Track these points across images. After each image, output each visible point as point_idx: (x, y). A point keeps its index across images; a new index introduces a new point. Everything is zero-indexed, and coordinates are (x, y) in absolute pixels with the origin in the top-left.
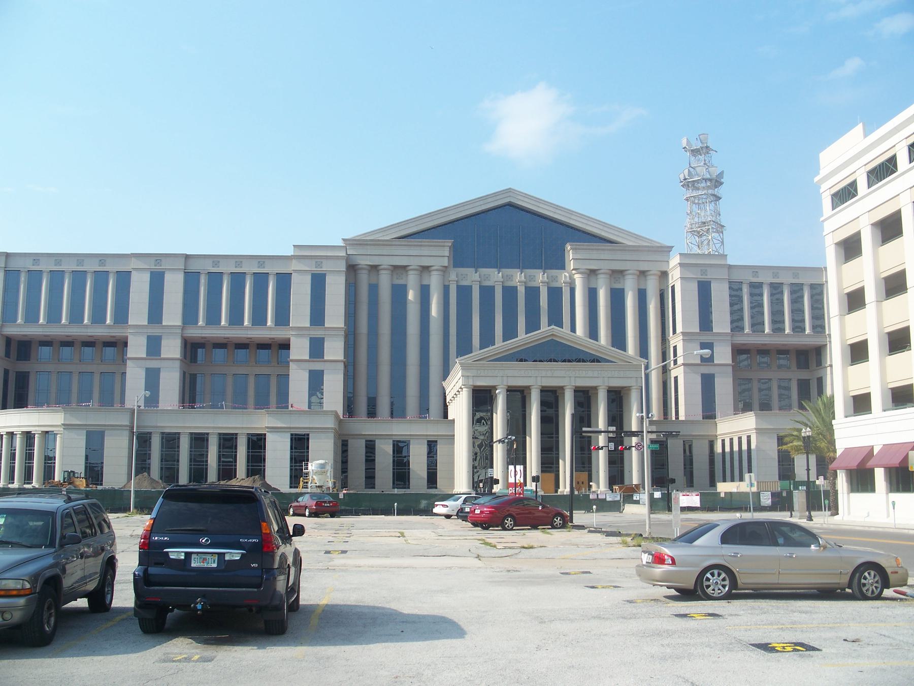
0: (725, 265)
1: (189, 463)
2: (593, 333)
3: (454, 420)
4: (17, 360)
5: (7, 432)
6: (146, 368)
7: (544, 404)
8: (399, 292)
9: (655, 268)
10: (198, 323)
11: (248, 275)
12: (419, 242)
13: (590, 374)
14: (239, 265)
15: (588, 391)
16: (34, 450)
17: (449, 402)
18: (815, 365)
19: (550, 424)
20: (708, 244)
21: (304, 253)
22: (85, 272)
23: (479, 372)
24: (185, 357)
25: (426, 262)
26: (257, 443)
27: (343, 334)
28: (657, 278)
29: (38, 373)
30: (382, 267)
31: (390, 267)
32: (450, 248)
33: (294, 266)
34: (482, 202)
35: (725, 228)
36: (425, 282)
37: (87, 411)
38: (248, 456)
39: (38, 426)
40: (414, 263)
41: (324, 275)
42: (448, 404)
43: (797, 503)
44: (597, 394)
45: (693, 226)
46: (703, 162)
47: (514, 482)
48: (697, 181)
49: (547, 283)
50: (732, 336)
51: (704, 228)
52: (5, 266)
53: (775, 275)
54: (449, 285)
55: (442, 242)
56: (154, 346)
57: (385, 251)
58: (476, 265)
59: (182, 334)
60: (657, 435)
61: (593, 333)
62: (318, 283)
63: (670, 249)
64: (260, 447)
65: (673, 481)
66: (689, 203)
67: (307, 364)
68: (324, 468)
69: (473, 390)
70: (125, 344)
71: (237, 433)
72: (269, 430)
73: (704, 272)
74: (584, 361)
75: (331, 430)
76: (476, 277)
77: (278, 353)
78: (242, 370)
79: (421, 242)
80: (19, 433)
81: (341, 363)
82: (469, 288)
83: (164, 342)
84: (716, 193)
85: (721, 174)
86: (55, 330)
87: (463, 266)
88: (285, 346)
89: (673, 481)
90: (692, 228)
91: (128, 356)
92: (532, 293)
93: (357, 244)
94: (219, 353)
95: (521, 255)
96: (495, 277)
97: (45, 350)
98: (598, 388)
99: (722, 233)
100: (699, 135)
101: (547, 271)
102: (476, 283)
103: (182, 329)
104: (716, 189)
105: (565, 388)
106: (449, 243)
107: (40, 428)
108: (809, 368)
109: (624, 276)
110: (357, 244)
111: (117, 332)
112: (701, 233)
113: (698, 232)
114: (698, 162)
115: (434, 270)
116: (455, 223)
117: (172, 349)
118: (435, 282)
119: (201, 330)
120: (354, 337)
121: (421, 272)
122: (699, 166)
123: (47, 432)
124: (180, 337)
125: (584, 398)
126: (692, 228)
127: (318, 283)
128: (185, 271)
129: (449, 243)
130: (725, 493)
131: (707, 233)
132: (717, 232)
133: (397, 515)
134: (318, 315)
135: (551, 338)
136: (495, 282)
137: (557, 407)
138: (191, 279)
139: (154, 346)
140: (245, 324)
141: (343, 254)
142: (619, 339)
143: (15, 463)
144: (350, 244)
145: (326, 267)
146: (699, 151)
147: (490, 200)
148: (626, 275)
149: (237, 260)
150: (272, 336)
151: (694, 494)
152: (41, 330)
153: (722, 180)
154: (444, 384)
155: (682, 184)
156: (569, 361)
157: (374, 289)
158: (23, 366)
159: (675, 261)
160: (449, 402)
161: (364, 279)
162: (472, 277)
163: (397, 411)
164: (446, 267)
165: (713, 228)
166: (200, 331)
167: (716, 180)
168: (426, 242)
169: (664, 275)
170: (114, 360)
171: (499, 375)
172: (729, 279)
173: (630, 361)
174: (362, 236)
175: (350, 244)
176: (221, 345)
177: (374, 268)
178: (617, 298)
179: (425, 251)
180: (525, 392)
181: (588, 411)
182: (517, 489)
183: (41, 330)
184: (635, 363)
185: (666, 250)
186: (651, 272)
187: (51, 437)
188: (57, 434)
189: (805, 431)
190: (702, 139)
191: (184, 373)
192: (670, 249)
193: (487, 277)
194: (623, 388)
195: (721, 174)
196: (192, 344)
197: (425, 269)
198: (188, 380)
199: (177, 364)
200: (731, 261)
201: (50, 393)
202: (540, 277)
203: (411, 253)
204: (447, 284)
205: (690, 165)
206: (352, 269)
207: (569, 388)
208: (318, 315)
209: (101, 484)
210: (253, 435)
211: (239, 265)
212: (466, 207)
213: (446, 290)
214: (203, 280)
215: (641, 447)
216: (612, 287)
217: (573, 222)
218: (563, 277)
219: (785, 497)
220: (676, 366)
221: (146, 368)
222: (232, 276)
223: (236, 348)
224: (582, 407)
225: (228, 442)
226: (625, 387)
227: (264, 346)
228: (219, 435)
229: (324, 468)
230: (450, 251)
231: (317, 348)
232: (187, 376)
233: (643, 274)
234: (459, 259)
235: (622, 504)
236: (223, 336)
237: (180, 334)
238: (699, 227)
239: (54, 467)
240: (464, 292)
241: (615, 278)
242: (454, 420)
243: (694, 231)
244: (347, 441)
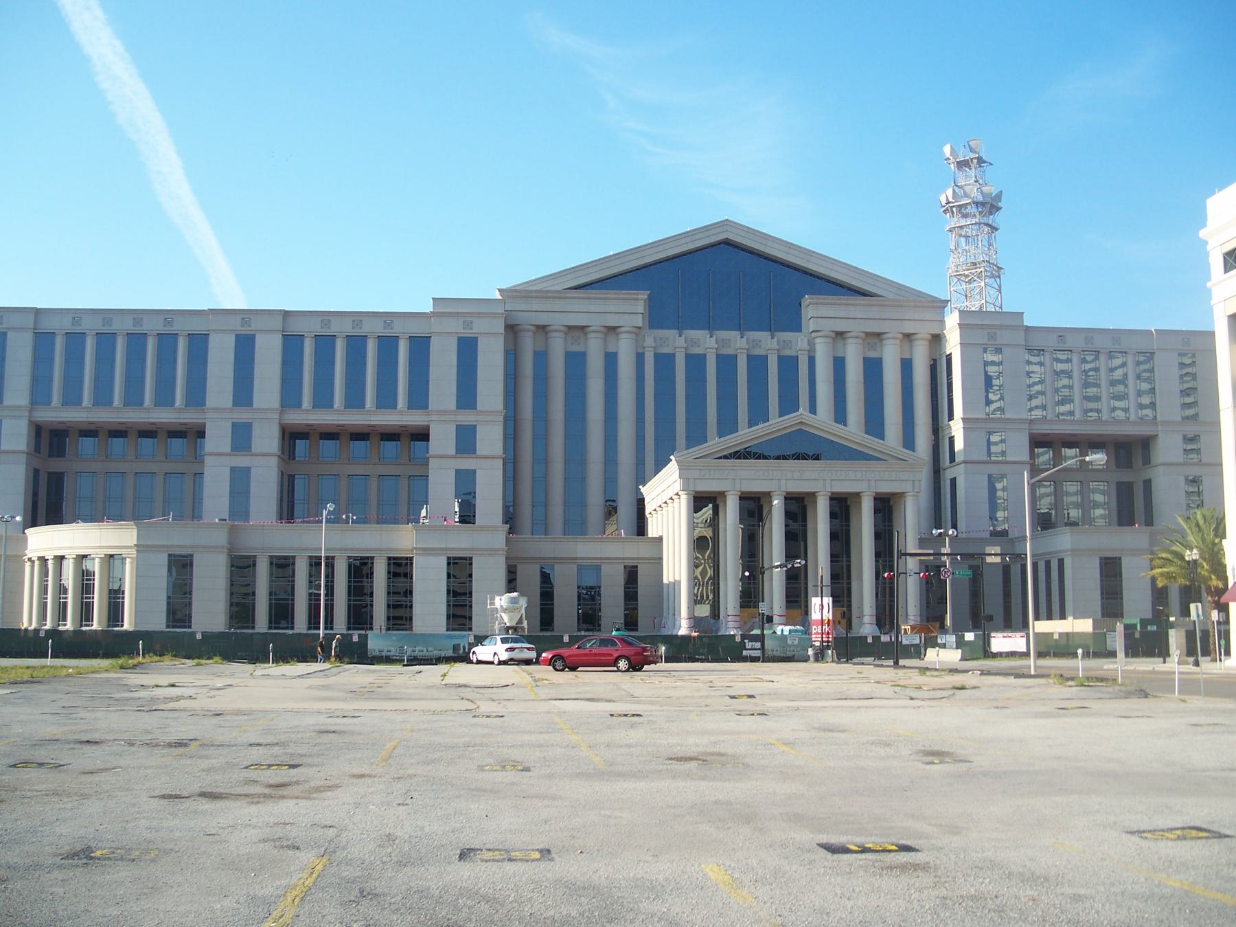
0: (1020, 326)
1: (308, 598)
2: (840, 415)
3: (660, 539)
4: (50, 456)
5: (54, 556)
6: (456, 470)
7: (789, 515)
8: (576, 363)
9: (924, 331)
10: (113, 403)
11: (308, 339)
12: (604, 293)
13: (851, 475)
14: (468, 325)
15: (846, 499)
16: (94, 580)
17: (650, 513)
18: (1140, 462)
19: (796, 540)
20: (980, 293)
21: (446, 308)
22: (364, 338)
23: (766, 474)
24: (37, 449)
25: (612, 321)
26: (400, 568)
27: (502, 420)
28: (926, 343)
29: (79, 474)
30: (591, 329)
31: (602, 329)
32: (645, 302)
33: (436, 326)
34: (688, 239)
35: (1002, 271)
36: (611, 349)
37: (342, 530)
38: (349, 587)
39: (100, 547)
40: (595, 322)
41: (253, 337)
42: (648, 516)
43: (1175, 644)
44: (860, 503)
45: (960, 268)
46: (974, 179)
47: (820, 618)
48: (965, 206)
49: (778, 350)
50: (1029, 423)
51: (973, 271)
52: (283, 328)
53: (388, 325)
54: (644, 353)
55: (634, 294)
56: (242, 437)
57: (558, 305)
58: (680, 325)
59: (280, 420)
60: (1002, 558)
61: (840, 415)
62: (467, 349)
63: (944, 305)
64: (1115, 576)
65: (990, 618)
66: (954, 235)
67: (452, 461)
68: (517, 603)
69: (694, 497)
70: (201, 434)
71: (374, 557)
72: (418, 552)
73: (468, 325)
74: (765, 458)
75: (222, 550)
76: (681, 341)
77: (196, 444)
78: (359, 470)
79: (606, 294)
80: (99, 556)
81: (274, 457)
82: (672, 357)
83: (256, 431)
84: (990, 222)
85: (999, 196)
86: (132, 415)
87: (662, 328)
88: (422, 435)
89: (990, 618)
90: (957, 271)
91: (206, 450)
92: (758, 364)
93: (517, 297)
94: (329, 446)
95: (711, 309)
96: (707, 342)
97: (88, 444)
98: (817, 494)
99: (1000, 278)
100: (968, 142)
101: (745, 333)
102: (773, 352)
103: (280, 414)
104: (991, 217)
105: (771, 494)
106: (644, 295)
107: (102, 550)
108: (1132, 467)
109: (881, 340)
110: (517, 297)
111: (190, 417)
112: (970, 278)
113: (967, 276)
114: (967, 179)
115: (889, 338)
116: (651, 267)
117: (267, 439)
118: (625, 349)
119: (307, 415)
120: (514, 424)
121: (606, 334)
122: (969, 185)
123: (112, 556)
124: (278, 424)
125: (842, 507)
126: (957, 271)
127: (467, 349)
128: (284, 333)
129: (644, 295)
130: (1060, 634)
131: (979, 277)
132: (993, 276)
133: (665, 662)
134: (467, 395)
135: (798, 428)
136: (768, 350)
137: (805, 519)
138: (292, 344)
139: (242, 437)
140: (367, 407)
141: (501, 310)
142: (874, 424)
143: (47, 598)
144: (509, 297)
145: (479, 327)
146: (969, 163)
147: (699, 236)
148: (884, 339)
149: (467, 319)
150: (404, 423)
151: (1018, 635)
152: (84, 415)
153: (1000, 204)
154: (643, 489)
155: (944, 209)
156: (785, 458)
157: (541, 358)
158: (56, 465)
159: (952, 321)
160: (650, 513)
161: (528, 345)
162: (676, 342)
163: (576, 526)
164: (639, 328)
165: (986, 271)
166: (54, 414)
167: (992, 204)
168: (612, 294)
169: (937, 339)
170: (124, 455)
171: (729, 477)
172: (1026, 346)
173: (904, 458)
174: (522, 286)
175: (509, 297)
176: (330, 434)
177: (542, 329)
178: (873, 369)
179: (612, 306)
180: (806, 500)
181: (846, 526)
182: (824, 627)
183: (84, 415)
184: (911, 461)
185: (940, 305)
186: (919, 336)
187: (117, 562)
188: (125, 558)
189: (1190, 553)
190: (973, 146)
191: (282, 473)
192: (944, 305)
193: (756, 343)
194: (893, 494)
195: (999, 196)
196: (51, 431)
197: (612, 330)
198: (286, 483)
199: (23, 458)
200: (1028, 321)
201: (154, 502)
202: (767, 343)
203: (592, 308)
204: (640, 351)
205: (955, 183)
206: (512, 330)
207: (867, 495)
208: (467, 395)
209: (292, 628)
210: (355, 558)
211: (326, 324)
212: (667, 246)
213: (640, 358)
214: (59, 343)
215: (949, 574)
216: (835, 355)
217: (812, 267)
218: (797, 343)
219: (1137, 639)
220: (953, 464)
221: (456, 470)
222: (189, 338)
223: (321, 439)
224: (795, 521)
225: (360, 569)
226: (897, 494)
227: (390, 435)
228: (310, 559)
229: (517, 603)
230: (645, 306)
231: (466, 440)
232: (286, 478)
233: (908, 337)
234: (657, 318)
235: (922, 649)
236: (336, 422)
237: (278, 421)
238: (968, 270)
239: (123, 603)
240: (665, 363)
241: (869, 344)
242: (660, 539)
243: (960, 275)
244: (515, 566)
